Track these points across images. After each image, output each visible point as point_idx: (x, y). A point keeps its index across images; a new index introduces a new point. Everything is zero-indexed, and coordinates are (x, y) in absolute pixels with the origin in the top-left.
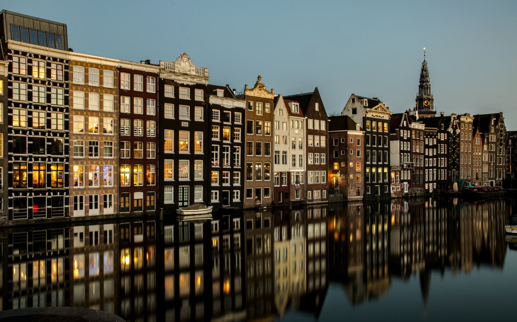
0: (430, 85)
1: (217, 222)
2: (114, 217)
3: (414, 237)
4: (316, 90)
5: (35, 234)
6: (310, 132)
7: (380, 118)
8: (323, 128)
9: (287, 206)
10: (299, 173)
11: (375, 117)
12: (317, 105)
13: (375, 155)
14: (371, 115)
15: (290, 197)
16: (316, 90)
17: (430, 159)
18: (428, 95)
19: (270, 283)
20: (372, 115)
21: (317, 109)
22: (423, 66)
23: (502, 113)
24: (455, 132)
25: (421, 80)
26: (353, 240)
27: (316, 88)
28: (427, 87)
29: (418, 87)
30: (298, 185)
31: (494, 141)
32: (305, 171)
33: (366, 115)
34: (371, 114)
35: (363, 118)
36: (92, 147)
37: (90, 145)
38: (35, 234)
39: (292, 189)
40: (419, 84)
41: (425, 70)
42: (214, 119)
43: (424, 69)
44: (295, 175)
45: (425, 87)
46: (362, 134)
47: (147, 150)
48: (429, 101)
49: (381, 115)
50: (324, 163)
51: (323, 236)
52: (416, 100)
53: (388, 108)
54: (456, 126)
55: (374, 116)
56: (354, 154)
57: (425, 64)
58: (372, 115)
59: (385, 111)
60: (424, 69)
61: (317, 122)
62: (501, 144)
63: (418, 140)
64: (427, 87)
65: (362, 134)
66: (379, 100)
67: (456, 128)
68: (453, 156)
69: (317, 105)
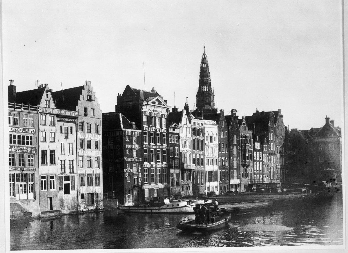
0: (211, 80)
1: (164, 183)
2: (288, 200)
5: (11, 156)
17: (258, 162)
19: (131, 208)
20: (149, 110)
22: (203, 58)
23: (279, 111)
26: (243, 210)
29: (198, 82)
38: (11, 156)
40: (199, 78)
41: (205, 63)
42: (237, 149)
43: (204, 62)
53: (166, 101)
57: (204, 56)
59: (163, 105)
60: (204, 62)
66: (156, 92)
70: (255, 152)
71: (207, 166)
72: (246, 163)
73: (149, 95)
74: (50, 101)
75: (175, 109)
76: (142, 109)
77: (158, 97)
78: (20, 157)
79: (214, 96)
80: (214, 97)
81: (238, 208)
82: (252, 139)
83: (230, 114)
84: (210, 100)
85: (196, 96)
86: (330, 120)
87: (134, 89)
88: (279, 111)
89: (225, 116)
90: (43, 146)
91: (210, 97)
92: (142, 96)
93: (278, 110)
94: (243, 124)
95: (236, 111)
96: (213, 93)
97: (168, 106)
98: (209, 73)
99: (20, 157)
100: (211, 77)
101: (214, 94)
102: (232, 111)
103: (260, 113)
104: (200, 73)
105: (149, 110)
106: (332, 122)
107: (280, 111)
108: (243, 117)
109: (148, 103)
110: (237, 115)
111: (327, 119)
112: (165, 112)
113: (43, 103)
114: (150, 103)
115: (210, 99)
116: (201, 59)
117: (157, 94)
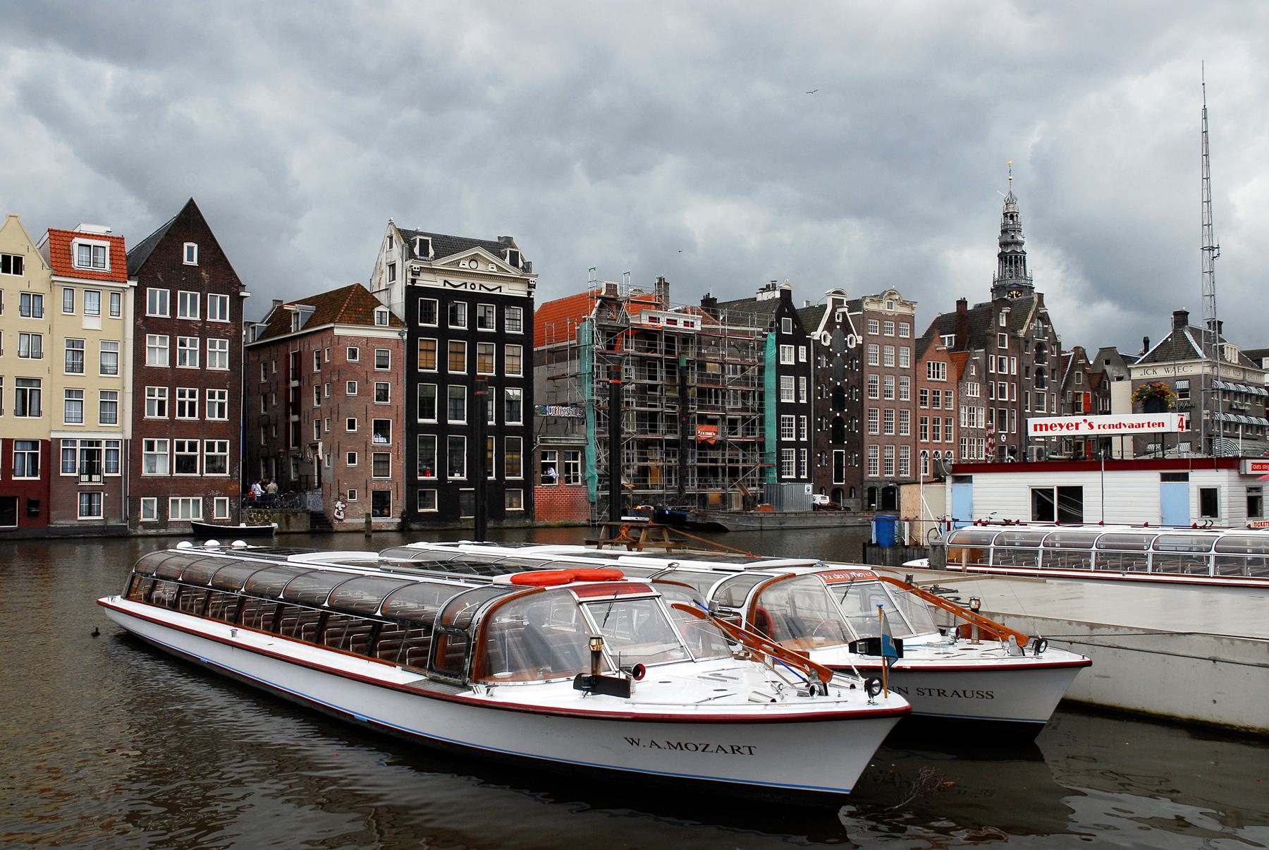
6: (145, 326)
9: (515, 605)
10: (98, 443)
13: (493, 400)
15: (53, 513)
18: (1022, 278)
24: (840, 342)
25: (1003, 240)
27: (191, 200)
28: (1016, 257)
30: (95, 478)
31: (1009, 371)
32: (129, 436)
33: (414, 281)
35: (407, 288)
39: (58, 492)
44: (78, 447)
45: (1011, 257)
46: (398, 337)
47: (507, 509)
48: (1021, 292)
49: (491, 285)
52: (992, 290)
54: (845, 324)
56: (364, 392)
58: (445, 281)
62: (1040, 383)
64: (1016, 257)
65: (398, 337)
67: (846, 329)
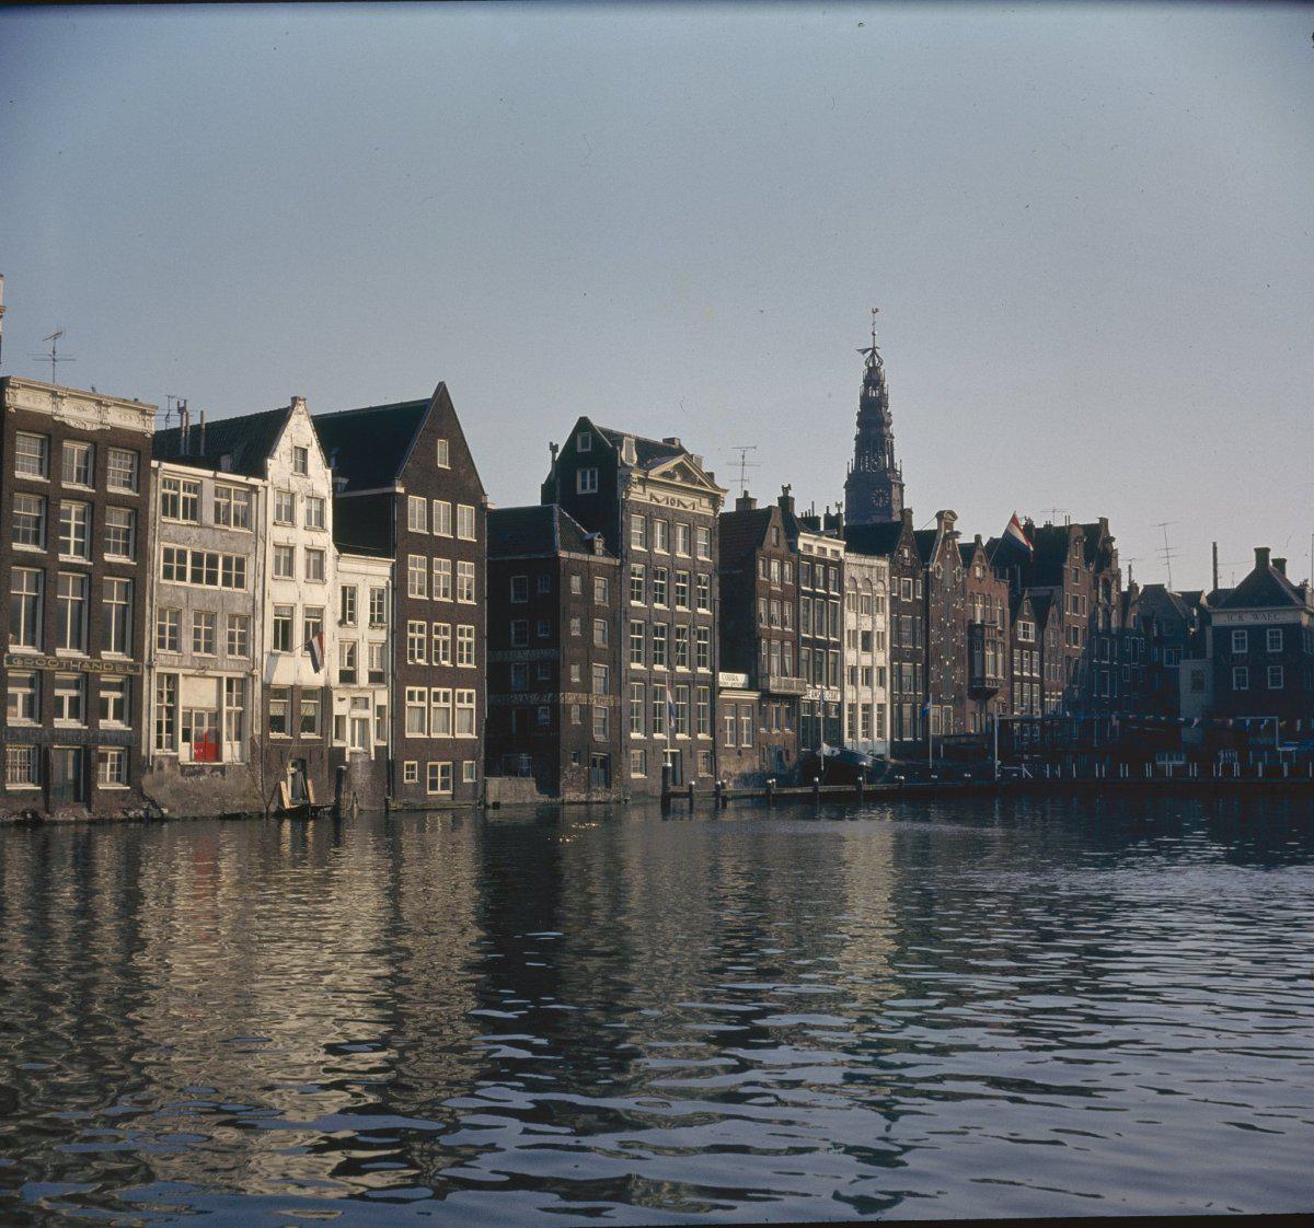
3: (388, 1152)
4: (442, 390)
7: (681, 508)
8: (466, 534)
11: (663, 504)
12: (442, 446)
14: (648, 497)
16: (442, 390)
20: (652, 497)
21: (443, 464)
23: (1104, 522)
34: (649, 490)
36: (234, 633)
37: (230, 627)
43: (873, 379)
50: (469, 661)
51: (883, 811)
53: (711, 475)
55: (685, 507)
57: (874, 361)
60: (873, 379)
61: (441, 506)
63: (821, 595)
68: (946, 659)
69: (442, 446)
70: (1016, 651)
71: (848, 688)
72: (984, 684)
73: (650, 452)
74: (310, 452)
75: (745, 502)
76: (628, 493)
77: (679, 459)
78: (200, 624)
79: (902, 486)
80: (902, 491)
81: (1051, 931)
82: (1008, 610)
83: (934, 526)
84: (890, 501)
85: (846, 486)
86: (1272, 556)
87: (603, 430)
88: (1104, 522)
89: (917, 533)
90: (282, 593)
91: (891, 490)
92: (629, 456)
93: (1097, 522)
94: (976, 558)
95: (955, 517)
96: (900, 479)
97: (715, 487)
98: (890, 414)
99: (200, 624)
100: (893, 429)
101: (904, 480)
102: (940, 516)
103: (1038, 529)
104: (859, 414)
105: (652, 497)
106: (1280, 563)
107: (1107, 526)
108: (978, 538)
109: (646, 474)
110: (955, 529)
111: (1262, 554)
112: (704, 507)
113: (279, 465)
114: (654, 474)
115: (890, 496)
116: (860, 371)
117: (681, 451)
